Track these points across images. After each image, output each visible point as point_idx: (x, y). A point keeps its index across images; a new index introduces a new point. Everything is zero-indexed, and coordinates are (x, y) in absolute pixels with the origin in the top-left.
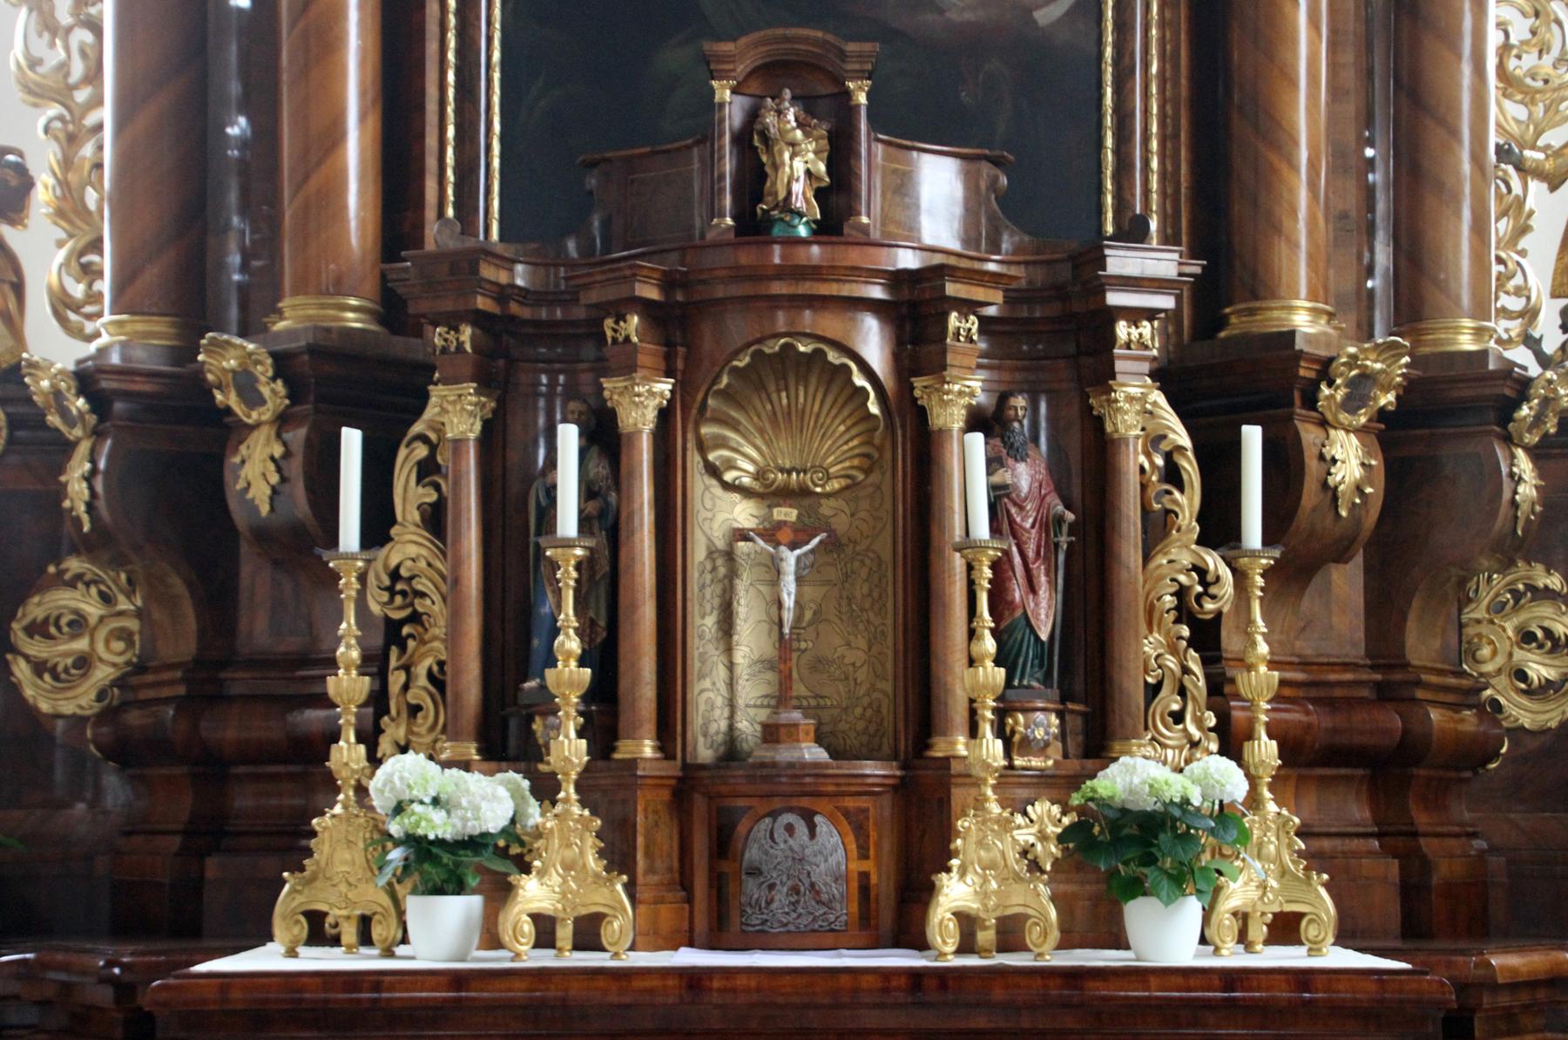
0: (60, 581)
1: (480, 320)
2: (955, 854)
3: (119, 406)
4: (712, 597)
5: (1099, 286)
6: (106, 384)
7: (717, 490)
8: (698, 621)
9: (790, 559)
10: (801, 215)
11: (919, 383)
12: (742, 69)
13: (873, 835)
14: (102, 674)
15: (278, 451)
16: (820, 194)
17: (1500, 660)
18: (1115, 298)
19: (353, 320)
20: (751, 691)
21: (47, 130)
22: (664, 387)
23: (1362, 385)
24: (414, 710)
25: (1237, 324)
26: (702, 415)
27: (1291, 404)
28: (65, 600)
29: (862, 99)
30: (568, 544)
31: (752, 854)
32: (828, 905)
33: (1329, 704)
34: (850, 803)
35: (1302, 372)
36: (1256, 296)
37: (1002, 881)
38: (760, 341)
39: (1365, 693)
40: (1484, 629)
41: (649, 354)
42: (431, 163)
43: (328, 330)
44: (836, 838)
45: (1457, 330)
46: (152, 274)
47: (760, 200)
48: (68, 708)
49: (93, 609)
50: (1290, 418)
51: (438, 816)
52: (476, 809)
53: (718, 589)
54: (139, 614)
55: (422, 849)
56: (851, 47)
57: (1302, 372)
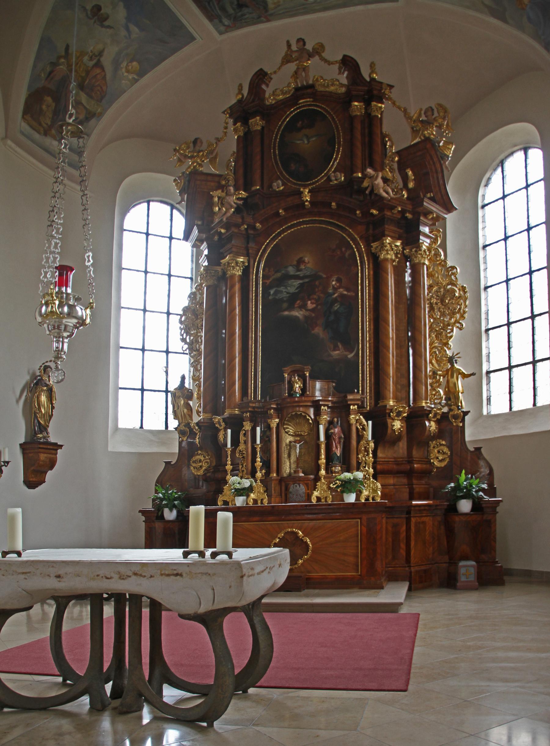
0: (198, 454)
1: (250, 412)
2: (317, 488)
3: (202, 428)
4: (286, 452)
5: (347, 401)
6: (200, 424)
7: (287, 435)
8: (283, 455)
9: (298, 445)
10: (297, 393)
11: (318, 417)
12: (290, 370)
13: (310, 487)
14: (204, 468)
15: (224, 433)
16: (301, 390)
17: (434, 456)
18: (349, 403)
19: (237, 412)
20: (293, 466)
21: (196, 385)
22: (277, 420)
23: (399, 414)
24: (243, 471)
25: (381, 404)
26: (284, 424)
27: (386, 416)
28: (198, 457)
29: (308, 375)
30: (258, 445)
31: (291, 490)
32: (302, 497)
33: (398, 464)
34: (306, 482)
35: (387, 412)
36: (383, 399)
37: (324, 492)
38: (292, 412)
39: (404, 462)
40: (432, 451)
41: (275, 415)
42: (249, 387)
43: (231, 414)
44: (303, 487)
45: (422, 403)
46: (208, 408)
47: (292, 391)
48: (199, 474)
49: (202, 459)
50: (386, 419)
51: (238, 485)
52: (244, 484)
53: (288, 451)
54: (209, 459)
55: (236, 490)
56: (305, 367)
57: (387, 412)
